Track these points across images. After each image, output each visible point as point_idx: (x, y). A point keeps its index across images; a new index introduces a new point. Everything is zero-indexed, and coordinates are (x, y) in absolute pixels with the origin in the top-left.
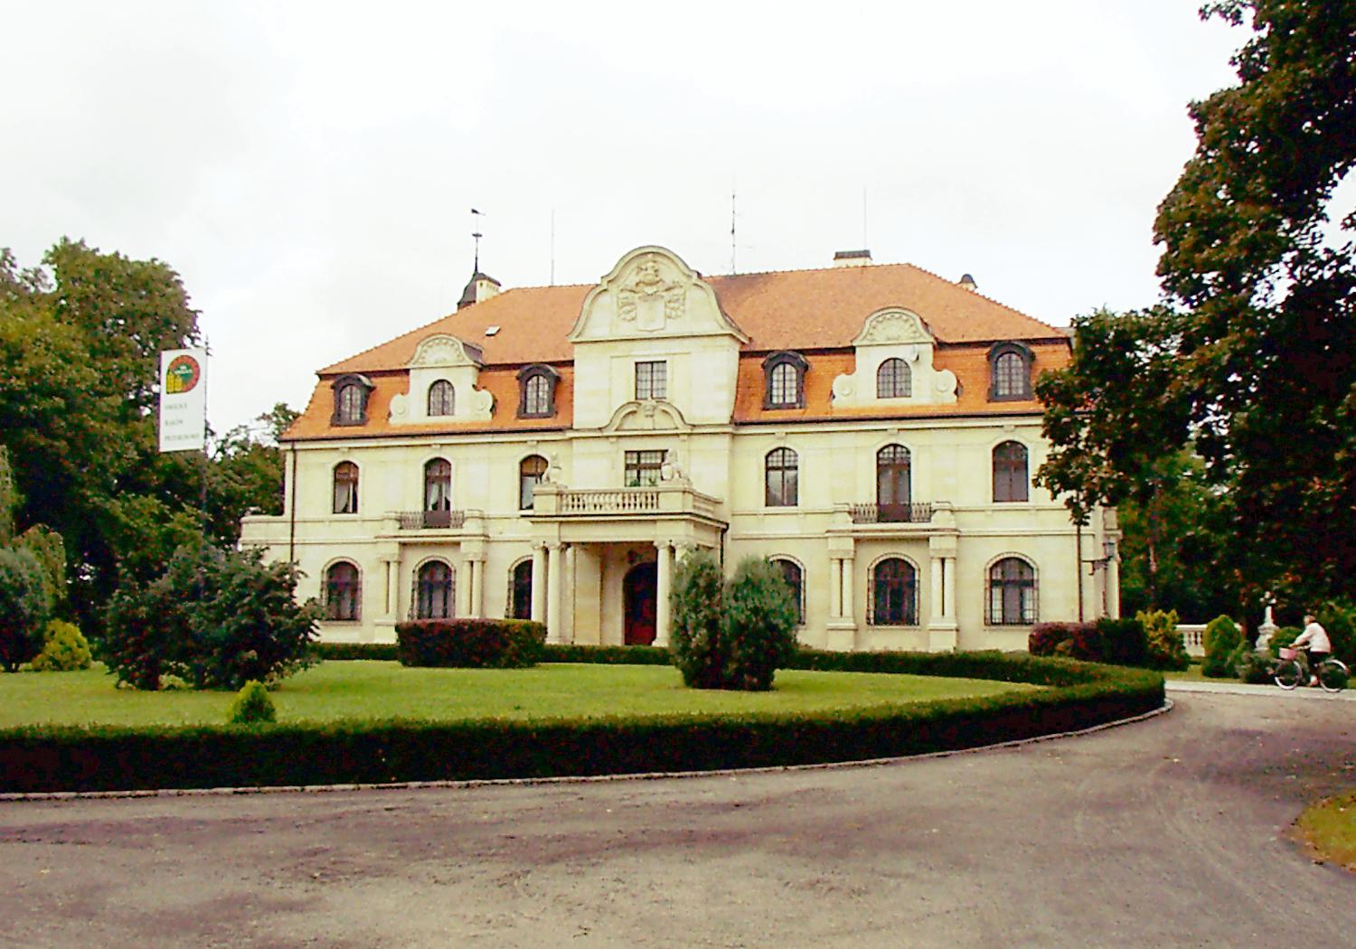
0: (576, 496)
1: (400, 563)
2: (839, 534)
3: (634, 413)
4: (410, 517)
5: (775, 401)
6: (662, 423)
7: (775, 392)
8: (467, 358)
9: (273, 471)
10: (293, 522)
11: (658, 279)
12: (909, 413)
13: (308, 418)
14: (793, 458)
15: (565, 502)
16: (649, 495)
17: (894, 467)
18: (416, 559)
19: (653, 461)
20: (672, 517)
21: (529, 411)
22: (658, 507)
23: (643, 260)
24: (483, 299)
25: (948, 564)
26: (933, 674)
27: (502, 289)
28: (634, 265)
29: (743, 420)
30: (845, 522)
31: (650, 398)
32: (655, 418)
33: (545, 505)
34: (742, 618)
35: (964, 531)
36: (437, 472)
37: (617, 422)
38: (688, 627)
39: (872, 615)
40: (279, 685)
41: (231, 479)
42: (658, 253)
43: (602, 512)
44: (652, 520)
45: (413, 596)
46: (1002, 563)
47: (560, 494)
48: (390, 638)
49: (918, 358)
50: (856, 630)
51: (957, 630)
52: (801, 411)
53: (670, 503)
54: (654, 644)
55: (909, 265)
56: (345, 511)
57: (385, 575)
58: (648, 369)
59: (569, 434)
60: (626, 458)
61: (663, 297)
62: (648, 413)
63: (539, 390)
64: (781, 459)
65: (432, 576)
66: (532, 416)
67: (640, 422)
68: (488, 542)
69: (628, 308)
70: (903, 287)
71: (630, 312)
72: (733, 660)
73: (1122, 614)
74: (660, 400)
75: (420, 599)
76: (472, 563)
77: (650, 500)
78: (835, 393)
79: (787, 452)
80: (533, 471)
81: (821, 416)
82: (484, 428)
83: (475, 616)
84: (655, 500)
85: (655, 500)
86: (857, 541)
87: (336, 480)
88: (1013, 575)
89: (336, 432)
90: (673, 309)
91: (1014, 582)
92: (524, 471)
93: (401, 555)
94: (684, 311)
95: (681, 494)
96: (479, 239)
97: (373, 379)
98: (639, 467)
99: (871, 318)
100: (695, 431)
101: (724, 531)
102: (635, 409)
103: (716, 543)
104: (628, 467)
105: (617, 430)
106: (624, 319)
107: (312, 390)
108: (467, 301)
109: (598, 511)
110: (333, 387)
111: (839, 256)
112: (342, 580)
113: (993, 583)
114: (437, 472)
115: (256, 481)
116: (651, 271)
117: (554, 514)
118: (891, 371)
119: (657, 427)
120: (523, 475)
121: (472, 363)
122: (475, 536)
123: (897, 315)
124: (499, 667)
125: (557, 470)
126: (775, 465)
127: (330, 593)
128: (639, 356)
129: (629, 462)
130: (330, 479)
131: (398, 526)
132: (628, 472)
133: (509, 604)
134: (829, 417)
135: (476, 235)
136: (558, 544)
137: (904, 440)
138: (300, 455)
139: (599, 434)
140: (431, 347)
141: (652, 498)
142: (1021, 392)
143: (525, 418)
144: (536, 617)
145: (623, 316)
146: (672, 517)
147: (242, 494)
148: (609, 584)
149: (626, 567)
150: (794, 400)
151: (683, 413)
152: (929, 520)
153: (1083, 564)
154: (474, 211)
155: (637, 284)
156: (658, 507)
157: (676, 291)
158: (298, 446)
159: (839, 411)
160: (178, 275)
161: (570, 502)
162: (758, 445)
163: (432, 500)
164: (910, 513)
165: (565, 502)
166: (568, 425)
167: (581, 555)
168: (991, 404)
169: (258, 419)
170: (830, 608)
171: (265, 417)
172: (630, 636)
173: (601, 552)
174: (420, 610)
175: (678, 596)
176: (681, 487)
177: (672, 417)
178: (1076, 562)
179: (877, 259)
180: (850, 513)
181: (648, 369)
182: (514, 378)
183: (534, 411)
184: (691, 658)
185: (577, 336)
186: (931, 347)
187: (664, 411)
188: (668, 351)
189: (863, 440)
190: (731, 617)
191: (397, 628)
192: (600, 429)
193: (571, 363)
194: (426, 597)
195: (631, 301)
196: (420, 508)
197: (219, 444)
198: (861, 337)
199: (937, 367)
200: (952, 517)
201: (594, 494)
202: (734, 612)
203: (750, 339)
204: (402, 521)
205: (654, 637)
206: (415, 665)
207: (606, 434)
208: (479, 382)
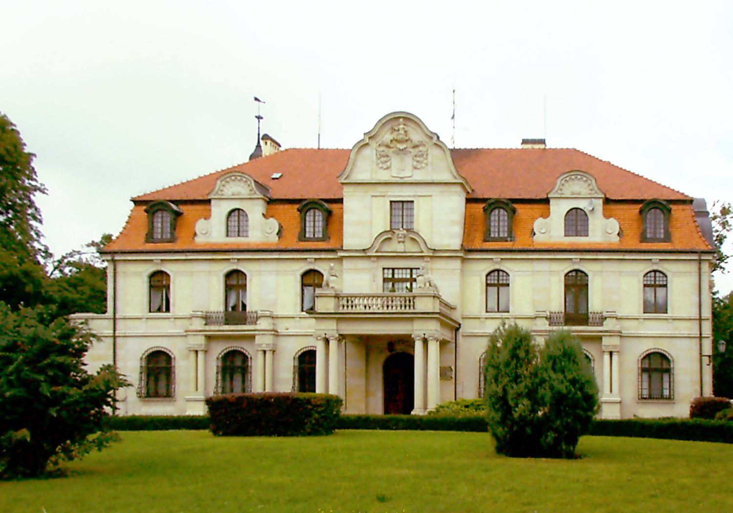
0: (350, 298)
1: (206, 352)
3: (389, 239)
4: (214, 315)
5: (492, 235)
6: (410, 248)
7: (492, 229)
8: (258, 193)
9: (99, 285)
10: (115, 319)
11: (407, 138)
12: (588, 248)
13: (126, 235)
14: (505, 278)
15: (341, 303)
16: (407, 298)
17: (577, 284)
18: (219, 349)
19: (404, 276)
20: (426, 316)
21: (307, 236)
22: (414, 308)
23: (395, 123)
24: (268, 154)
25: (615, 357)
26: (607, 434)
27: (282, 149)
28: (388, 127)
29: (470, 248)
30: (198, 324)
31: (401, 229)
33: (325, 305)
34: (563, 388)
36: (235, 281)
38: (509, 397)
40: (66, 469)
41: (66, 289)
42: (409, 119)
43: (371, 311)
44: (411, 318)
45: (217, 377)
46: (648, 356)
47: (337, 297)
48: (200, 410)
49: (593, 209)
50: (620, 402)
52: (511, 243)
53: (423, 305)
54: (413, 413)
55: (575, 150)
56: (159, 310)
57: (195, 363)
58: (401, 208)
59: (341, 254)
60: (384, 274)
61: (410, 152)
64: (496, 278)
65: (232, 362)
66: (309, 240)
67: (395, 247)
68: (277, 335)
69: (385, 159)
70: (576, 163)
71: (386, 162)
72: (551, 429)
73: (716, 392)
75: (224, 379)
76: (265, 352)
77: (408, 303)
78: (535, 230)
79: (501, 273)
80: (311, 282)
81: (526, 247)
82: (273, 248)
83: (268, 390)
84: (412, 303)
85: (412, 303)
86: (209, 338)
87: (151, 287)
88: (656, 363)
89: (150, 246)
90: (418, 161)
91: (656, 370)
92: (305, 282)
93: (207, 345)
94: (427, 164)
95: (432, 298)
96: (261, 120)
97: (181, 207)
99: (561, 178)
100: (436, 255)
101: (457, 329)
102: (390, 236)
103: (452, 338)
104: (385, 280)
105: (376, 252)
106: (381, 168)
107: (129, 213)
108: (256, 154)
109: (367, 310)
110: (146, 211)
111: (525, 142)
112: (159, 369)
113: (644, 370)
114: (235, 281)
115: (87, 290)
116: (402, 132)
117: (333, 311)
118: (574, 218)
119: (407, 251)
120: (303, 285)
121: (262, 197)
122: (267, 331)
124: (303, 435)
125: (335, 278)
126: (492, 282)
127: (148, 376)
128: (394, 196)
129: (386, 276)
130: (146, 286)
131: (204, 323)
132: (386, 284)
133: (294, 384)
134: (532, 248)
137: (584, 267)
138: (121, 268)
139: (364, 254)
140: (227, 182)
141: (410, 301)
142: (662, 236)
143: (305, 241)
145: (380, 165)
146: (426, 316)
147: (74, 301)
148: (372, 369)
149: (382, 358)
150: (506, 235)
151: (427, 242)
152: (602, 325)
153: (703, 358)
154: (256, 99)
155: (391, 141)
156: (414, 308)
157: (421, 148)
158: (117, 258)
159: (539, 244)
160: (15, 125)
161: (345, 303)
162: (480, 269)
163: (232, 303)
164: (588, 318)
165: (341, 303)
166: (339, 247)
168: (644, 244)
169: (88, 246)
171: (93, 244)
172: (389, 404)
173: (366, 343)
174: (223, 388)
175: (497, 367)
176: (431, 292)
177: (420, 246)
178: (698, 355)
179: (550, 145)
180: (546, 318)
181: (401, 208)
182: (296, 210)
184: (511, 427)
185: (346, 179)
186: (601, 201)
187: (413, 239)
188: (414, 194)
189: (555, 266)
190: (552, 388)
191: (209, 402)
193: (340, 201)
194: (228, 379)
196: (222, 308)
197: (56, 264)
198: (554, 192)
199: (607, 216)
200: (618, 323)
201: (369, 297)
202: (555, 384)
203: (473, 190)
204: (207, 319)
205: (412, 407)
206: (225, 434)
207: (368, 254)
208: (267, 212)
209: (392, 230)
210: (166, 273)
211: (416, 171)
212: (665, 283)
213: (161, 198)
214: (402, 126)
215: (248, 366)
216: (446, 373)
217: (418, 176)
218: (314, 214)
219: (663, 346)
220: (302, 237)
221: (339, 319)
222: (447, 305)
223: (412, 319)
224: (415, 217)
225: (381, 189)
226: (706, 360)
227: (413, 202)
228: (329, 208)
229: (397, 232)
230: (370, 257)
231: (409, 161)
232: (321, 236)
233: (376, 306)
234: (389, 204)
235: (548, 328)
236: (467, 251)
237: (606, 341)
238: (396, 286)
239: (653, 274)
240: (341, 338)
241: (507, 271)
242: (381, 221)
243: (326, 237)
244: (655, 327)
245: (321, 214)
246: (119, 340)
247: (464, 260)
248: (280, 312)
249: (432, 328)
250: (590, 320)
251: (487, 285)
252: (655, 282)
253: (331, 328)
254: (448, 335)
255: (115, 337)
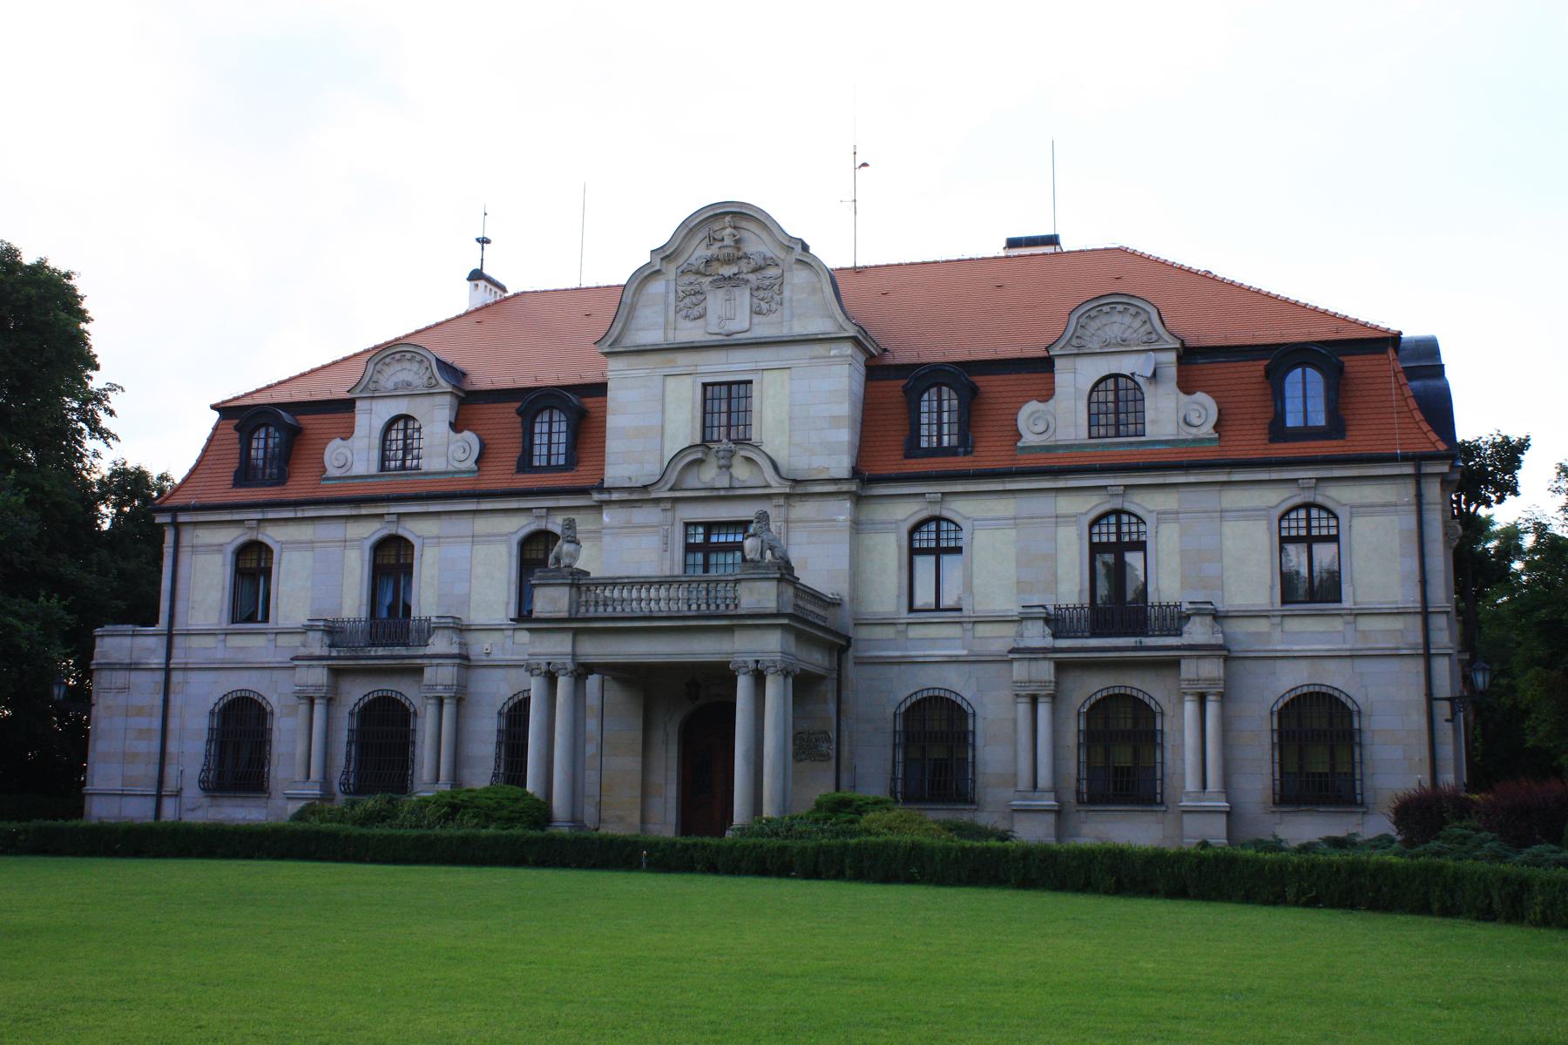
2: (1031, 653)
5: (924, 444)
8: (442, 382)
17: (392, 563)
18: (356, 692)
20: (757, 621)
27: (510, 293)
30: (1037, 635)
32: (733, 470)
35: (1237, 649)
37: (672, 477)
39: (1084, 788)
49: (1154, 374)
50: (1228, 813)
51: (1228, 813)
60: (686, 535)
62: (723, 462)
63: (551, 435)
64: (933, 536)
66: (539, 469)
69: (694, 299)
74: (744, 441)
76: (440, 701)
79: (944, 525)
86: (1061, 666)
98: (707, 548)
100: (799, 489)
102: (700, 455)
104: (690, 548)
105: (671, 489)
110: (237, 428)
111: (1013, 243)
116: (728, 241)
123: (1120, 307)
135: (484, 241)
136: (570, 667)
138: (187, 537)
139: (639, 495)
144: (532, 785)
146: (757, 621)
157: (772, 272)
158: (182, 518)
167: (616, 694)
168: (1276, 446)
170: (1015, 775)
172: (686, 824)
178: (1423, 699)
179: (1067, 244)
183: (544, 463)
187: (748, 459)
189: (1066, 504)
192: (645, 487)
195: (697, 288)
196: (364, 613)
201: (642, 584)
204: (1057, 622)
207: (653, 496)
209: (705, 442)
210: (406, 540)
211: (757, 319)
212: (1333, 532)
213: (282, 397)
214: (729, 230)
215: (966, 733)
216: (804, 746)
217: (763, 329)
218: (940, 401)
219: (1336, 678)
220: (525, 463)
221: (576, 633)
222: (816, 597)
223: (729, 630)
224: (755, 414)
225: (684, 360)
226: (1444, 710)
227: (750, 382)
228: (581, 406)
229: (715, 446)
230: (657, 501)
231: (743, 297)
232: (562, 461)
233: (660, 601)
234: (699, 390)
235: (1049, 642)
236: (865, 480)
237: (1188, 669)
238: (713, 558)
239: (1302, 514)
240: (581, 670)
241: (1140, 512)
242: (682, 427)
243: (572, 461)
244: (1311, 632)
245: (563, 418)
246: (176, 677)
247: (858, 499)
248: (476, 617)
249: (770, 645)
250: (1153, 623)
251: (1284, 541)
252: (1305, 529)
253: (559, 649)
254: (816, 660)
255: (168, 671)
